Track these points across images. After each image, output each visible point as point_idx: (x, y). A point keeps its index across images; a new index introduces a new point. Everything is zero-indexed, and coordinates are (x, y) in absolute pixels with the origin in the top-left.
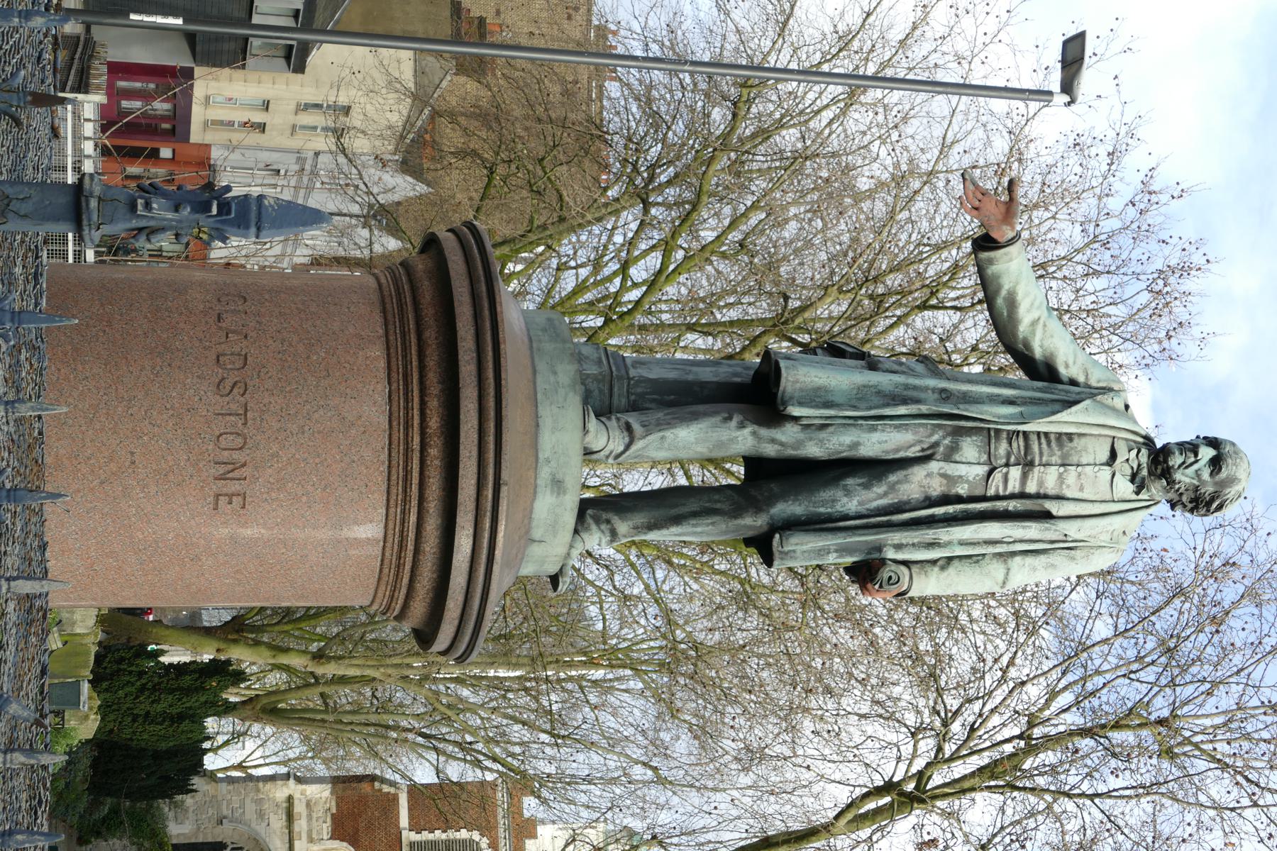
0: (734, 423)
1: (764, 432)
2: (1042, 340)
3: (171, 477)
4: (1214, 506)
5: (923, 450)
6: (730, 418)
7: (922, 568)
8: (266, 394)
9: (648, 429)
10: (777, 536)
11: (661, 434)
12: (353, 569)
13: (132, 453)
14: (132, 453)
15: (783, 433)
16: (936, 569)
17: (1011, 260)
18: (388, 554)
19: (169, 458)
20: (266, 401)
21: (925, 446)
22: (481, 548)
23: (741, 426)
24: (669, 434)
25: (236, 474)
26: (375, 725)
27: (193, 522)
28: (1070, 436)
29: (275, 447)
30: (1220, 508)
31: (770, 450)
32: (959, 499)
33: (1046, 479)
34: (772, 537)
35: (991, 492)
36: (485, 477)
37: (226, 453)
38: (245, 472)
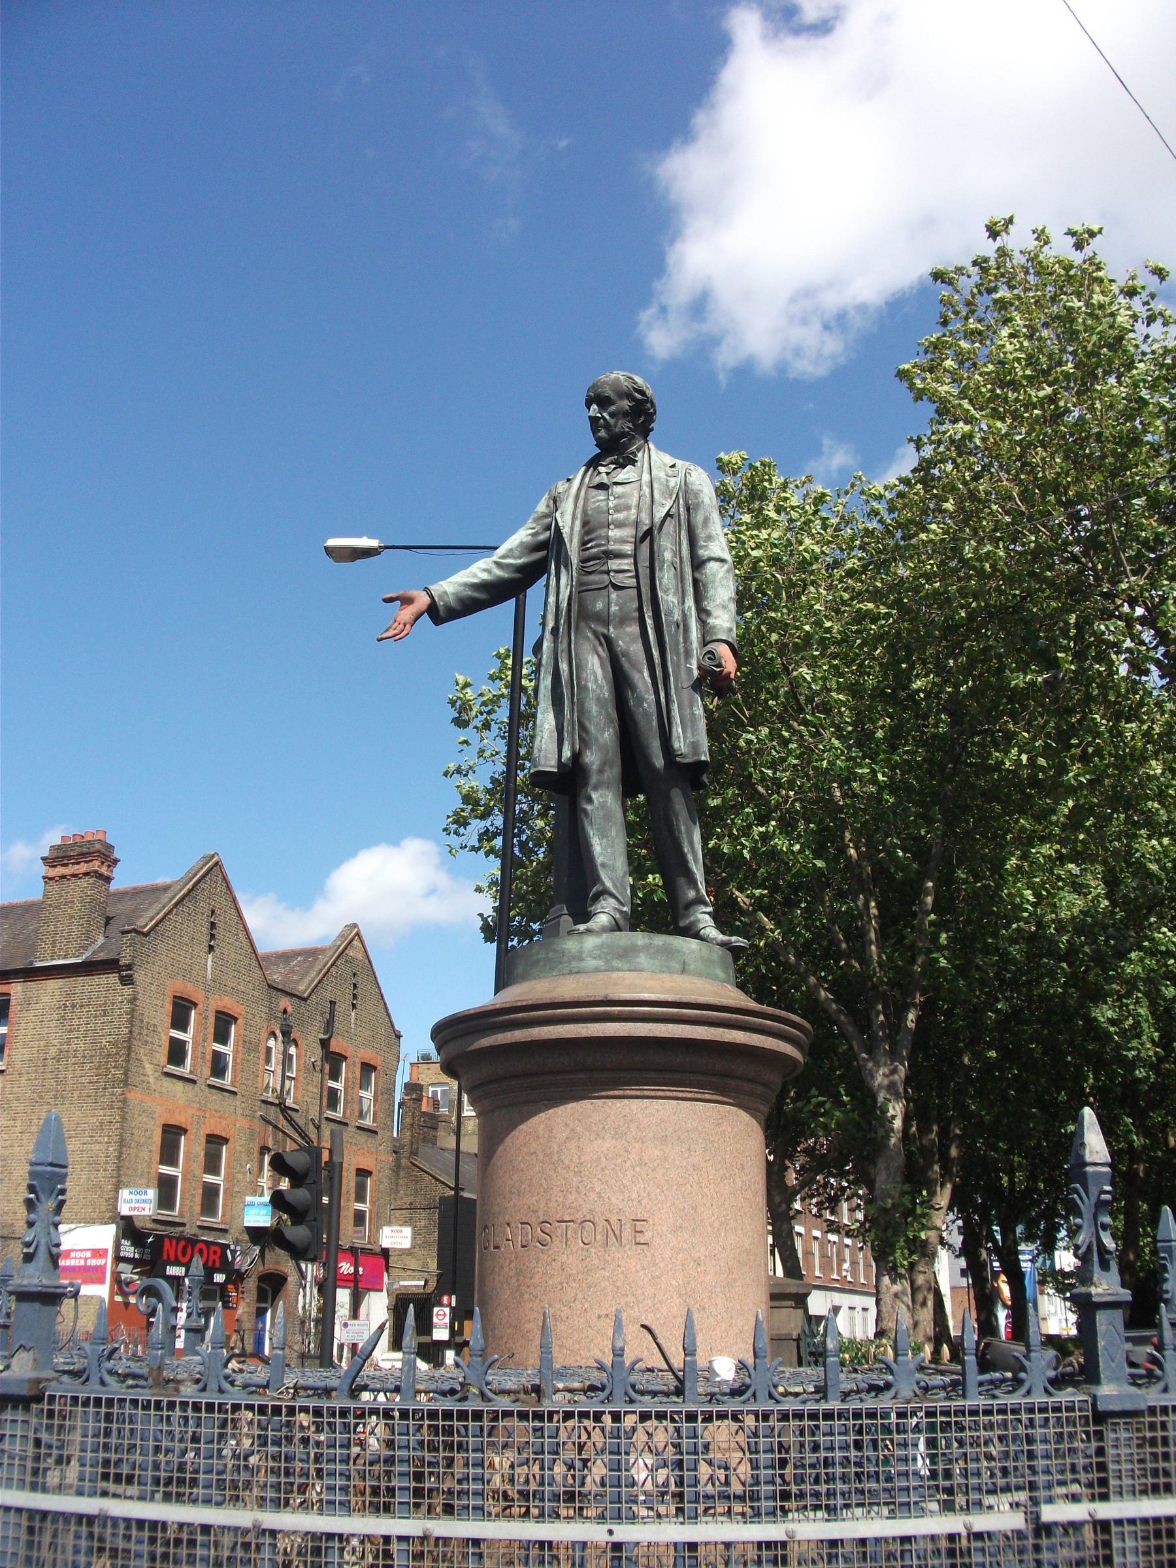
0: (589, 807)
1: (594, 779)
2: (515, 558)
3: (619, 1284)
4: (639, 397)
5: (601, 644)
6: (585, 811)
7: (708, 631)
8: (550, 1204)
9: (597, 879)
10: (678, 759)
11: (600, 868)
12: (707, 1125)
13: (599, 1317)
14: (599, 1317)
15: (593, 763)
16: (711, 621)
17: (445, 592)
18: (689, 1095)
19: (603, 1285)
20: (555, 1204)
21: (597, 643)
22: (673, 1014)
23: (590, 800)
24: (599, 860)
25: (616, 1228)
26: (764, 1085)
27: (661, 1265)
28: (585, 524)
29: (593, 1196)
30: (642, 393)
31: (614, 772)
32: (640, 609)
33: (620, 537)
34: (679, 764)
35: (633, 582)
36: (605, 1013)
37: (598, 1237)
38: (614, 1219)
